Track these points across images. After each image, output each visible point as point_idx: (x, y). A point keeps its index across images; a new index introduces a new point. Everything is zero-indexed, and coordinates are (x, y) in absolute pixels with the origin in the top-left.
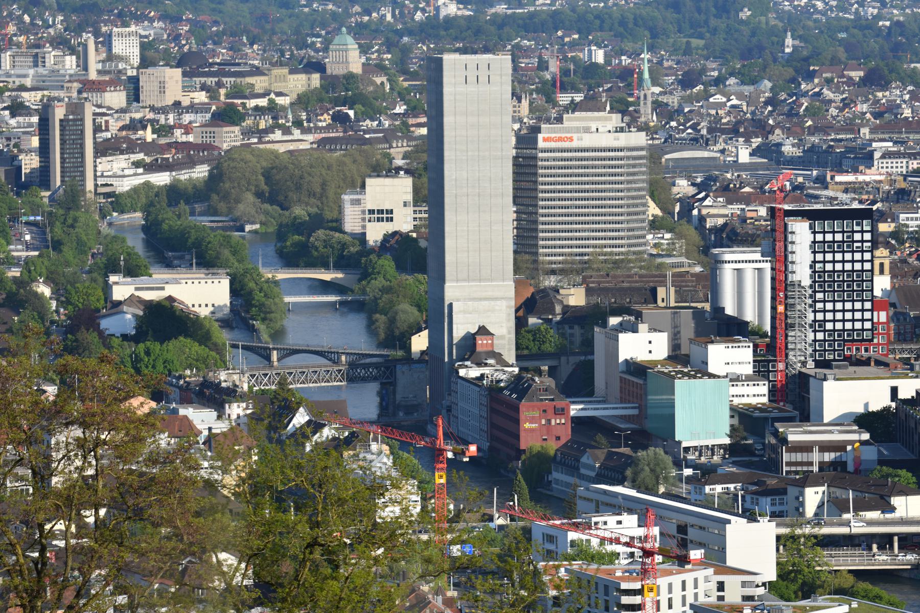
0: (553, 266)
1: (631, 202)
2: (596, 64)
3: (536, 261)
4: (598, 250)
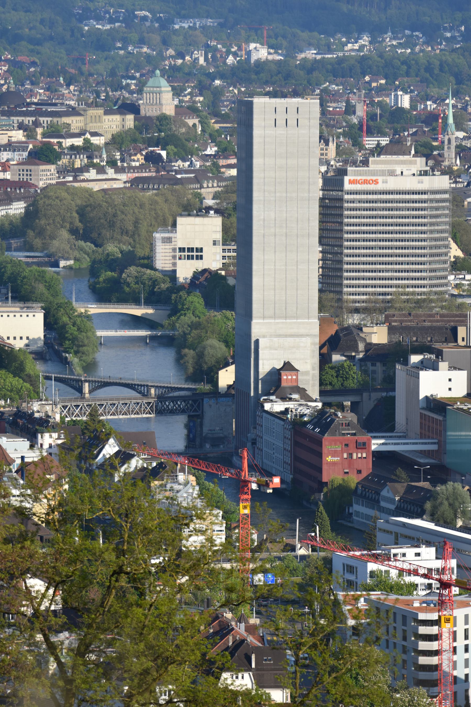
0: (357, 305)
1: (434, 243)
2: (402, 109)
4: (400, 290)
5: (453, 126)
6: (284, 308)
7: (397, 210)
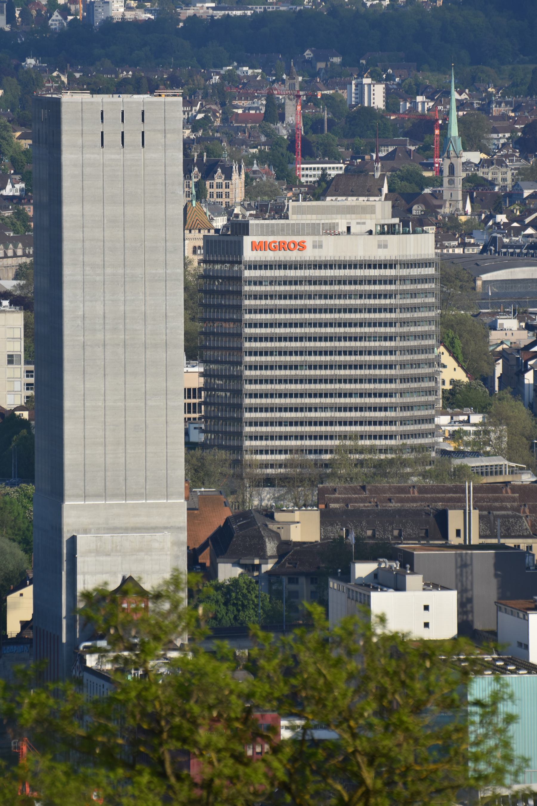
0: (269, 471)
1: (408, 357)
2: (370, 110)
3: (237, 463)
4: (348, 443)
5: (459, 142)
6: (122, 478)
7: (340, 297)
